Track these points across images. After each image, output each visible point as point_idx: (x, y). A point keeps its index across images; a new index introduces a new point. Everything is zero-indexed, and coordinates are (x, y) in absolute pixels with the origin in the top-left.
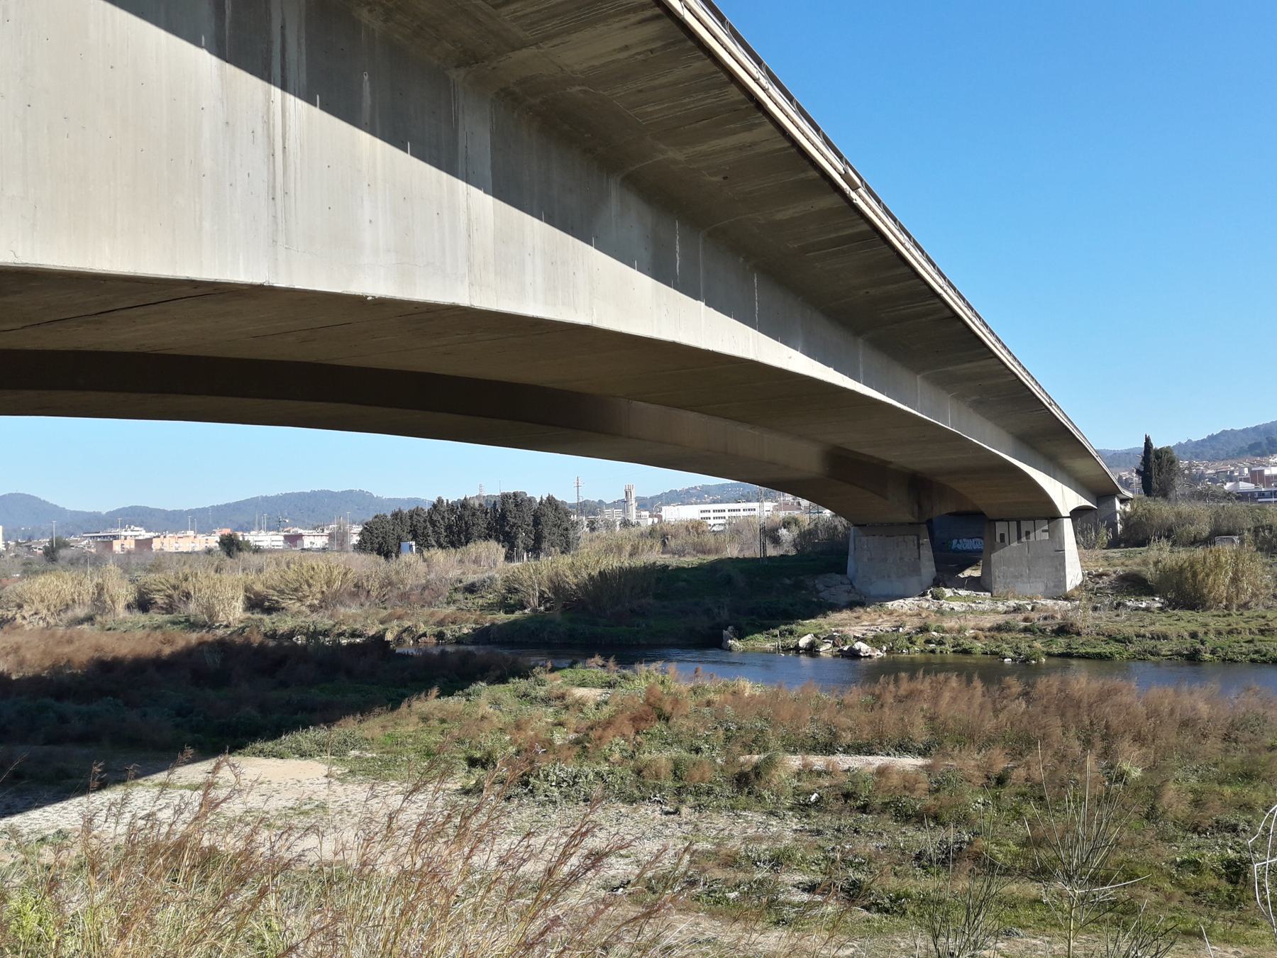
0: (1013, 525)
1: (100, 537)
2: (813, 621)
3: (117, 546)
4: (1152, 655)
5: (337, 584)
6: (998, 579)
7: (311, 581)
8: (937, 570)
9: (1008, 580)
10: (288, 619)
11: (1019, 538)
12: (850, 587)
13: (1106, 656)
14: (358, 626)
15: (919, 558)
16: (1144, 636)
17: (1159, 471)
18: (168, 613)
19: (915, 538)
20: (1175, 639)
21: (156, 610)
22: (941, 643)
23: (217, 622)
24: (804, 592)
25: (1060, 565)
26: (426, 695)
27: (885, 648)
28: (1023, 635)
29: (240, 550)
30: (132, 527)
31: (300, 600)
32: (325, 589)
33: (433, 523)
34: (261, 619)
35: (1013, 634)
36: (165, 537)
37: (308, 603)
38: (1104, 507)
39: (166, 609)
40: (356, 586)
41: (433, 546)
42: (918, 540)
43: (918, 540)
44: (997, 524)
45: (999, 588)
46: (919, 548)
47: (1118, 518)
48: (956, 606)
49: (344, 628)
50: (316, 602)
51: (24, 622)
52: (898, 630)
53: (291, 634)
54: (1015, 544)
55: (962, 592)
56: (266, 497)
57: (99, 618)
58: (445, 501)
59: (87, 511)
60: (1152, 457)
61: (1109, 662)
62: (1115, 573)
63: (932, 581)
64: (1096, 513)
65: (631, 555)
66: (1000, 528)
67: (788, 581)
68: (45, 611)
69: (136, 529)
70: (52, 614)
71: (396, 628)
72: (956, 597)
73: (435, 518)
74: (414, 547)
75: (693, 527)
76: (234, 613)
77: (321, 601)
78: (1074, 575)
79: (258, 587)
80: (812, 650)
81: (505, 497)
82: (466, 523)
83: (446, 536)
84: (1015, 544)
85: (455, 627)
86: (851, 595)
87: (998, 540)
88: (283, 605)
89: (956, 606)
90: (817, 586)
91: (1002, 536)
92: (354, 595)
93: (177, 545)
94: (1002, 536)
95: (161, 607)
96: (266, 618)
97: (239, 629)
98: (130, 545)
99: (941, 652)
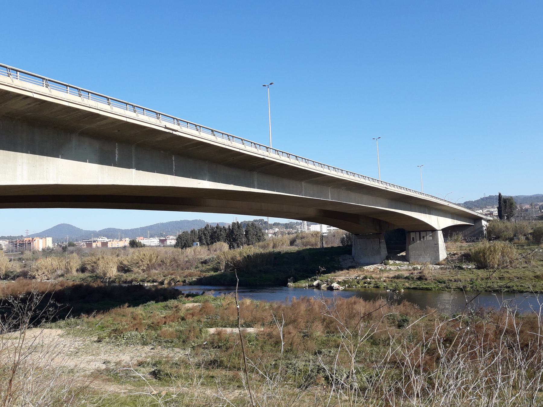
0: (418, 234)
1: (89, 241)
2: (329, 274)
3: (94, 245)
4: (448, 288)
5: (154, 261)
6: (412, 256)
7: (143, 260)
8: (388, 253)
9: (416, 257)
10: (133, 275)
11: (420, 239)
12: (353, 260)
13: (429, 289)
14: (155, 278)
15: (380, 248)
16: (451, 280)
17: (505, 208)
18: (92, 273)
19: (378, 239)
20: (464, 282)
21: (87, 272)
22: (369, 283)
23: (106, 277)
24: (334, 262)
25: (437, 250)
26: (123, 306)
27: (347, 286)
28: (404, 280)
29: (137, 246)
30: (102, 237)
31: (139, 267)
32: (148, 263)
33: (205, 235)
34: (122, 275)
35: (401, 280)
36: (113, 241)
37: (142, 268)
38: (477, 224)
39: (91, 271)
40: (161, 261)
41: (204, 244)
42: (380, 241)
43: (380, 241)
44: (411, 233)
45: (412, 260)
46: (380, 243)
47: (484, 228)
48: (392, 268)
49: (150, 278)
50: (145, 268)
51: (39, 277)
52: (357, 278)
53: (131, 281)
54: (418, 242)
55: (397, 262)
56: (162, 223)
57: (66, 275)
58: (210, 226)
59: (91, 230)
60: (502, 200)
61: (431, 291)
62: (460, 253)
63: (386, 257)
64: (474, 227)
65: (273, 247)
66: (412, 235)
67: (328, 258)
68: (47, 273)
69: (104, 238)
70: (50, 274)
71: (169, 279)
72: (395, 264)
73: (205, 232)
74: (198, 244)
75: (315, 234)
76: (113, 272)
77: (147, 268)
78: (443, 255)
79: (125, 263)
80: (318, 287)
81: (234, 223)
82: (218, 234)
83: (210, 240)
84: (418, 242)
85: (190, 278)
86: (353, 263)
87: (412, 240)
88: (132, 269)
89: (392, 268)
90: (340, 260)
91: (413, 238)
92: (160, 265)
93: (118, 244)
94: (413, 238)
95: (89, 271)
96: (124, 275)
97: (114, 279)
98: (99, 244)
99: (368, 287)
